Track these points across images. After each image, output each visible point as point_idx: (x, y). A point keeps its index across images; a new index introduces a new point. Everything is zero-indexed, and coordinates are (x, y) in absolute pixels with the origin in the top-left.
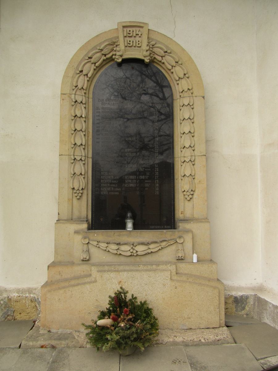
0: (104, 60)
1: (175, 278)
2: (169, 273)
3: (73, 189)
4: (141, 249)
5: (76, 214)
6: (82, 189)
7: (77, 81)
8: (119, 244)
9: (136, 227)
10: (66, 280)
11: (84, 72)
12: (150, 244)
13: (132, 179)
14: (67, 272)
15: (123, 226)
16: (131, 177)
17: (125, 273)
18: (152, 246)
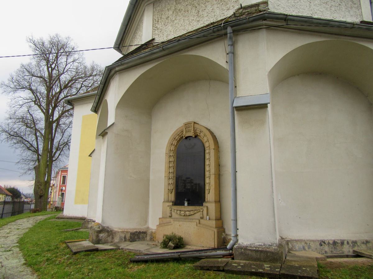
0: (180, 138)
1: (198, 225)
2: (196, 223)
3: (169, 189)
4: (187, 213)
5: (170, 199)
6: (172, 190)
7: (171, 148)
8: (180, 211)
9: (189, 204)
10: (164, 223)
11: (173, 144)
12: (304, 240)
13: (189, 185)
14: (165, 221)
15: (183, 204)
16: (189, 184)
17: (181, 222)
18: (191, 212)
